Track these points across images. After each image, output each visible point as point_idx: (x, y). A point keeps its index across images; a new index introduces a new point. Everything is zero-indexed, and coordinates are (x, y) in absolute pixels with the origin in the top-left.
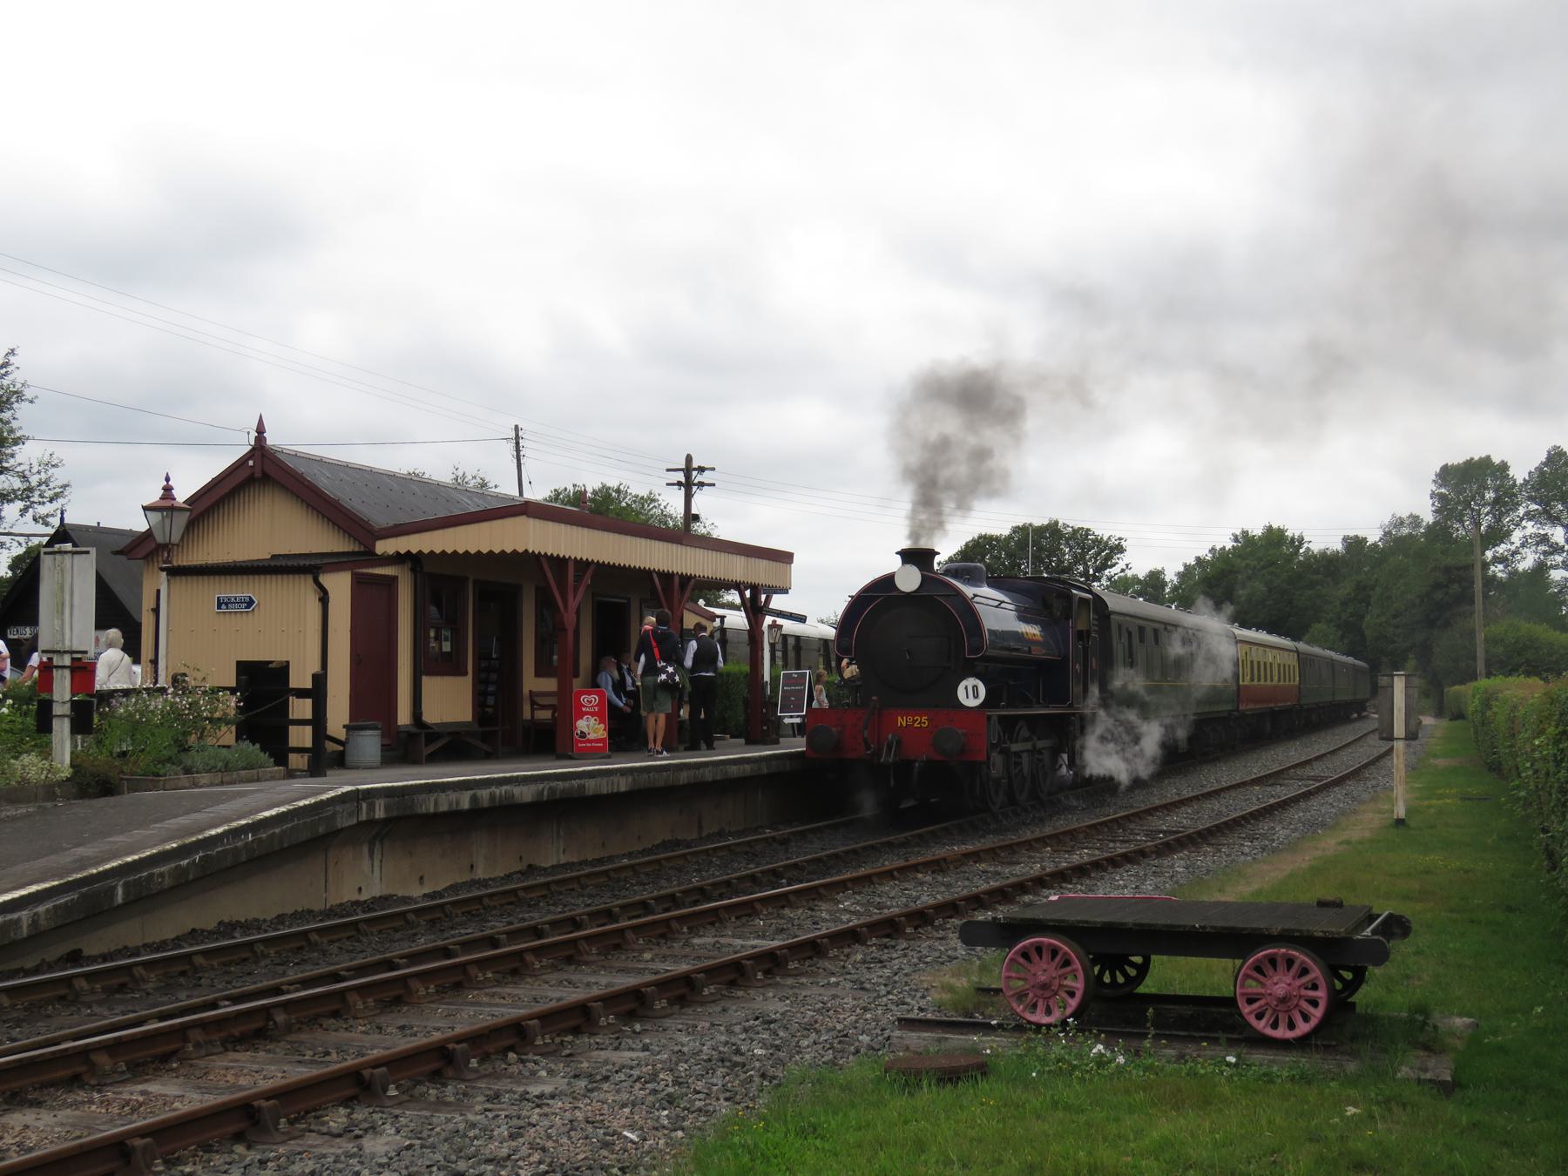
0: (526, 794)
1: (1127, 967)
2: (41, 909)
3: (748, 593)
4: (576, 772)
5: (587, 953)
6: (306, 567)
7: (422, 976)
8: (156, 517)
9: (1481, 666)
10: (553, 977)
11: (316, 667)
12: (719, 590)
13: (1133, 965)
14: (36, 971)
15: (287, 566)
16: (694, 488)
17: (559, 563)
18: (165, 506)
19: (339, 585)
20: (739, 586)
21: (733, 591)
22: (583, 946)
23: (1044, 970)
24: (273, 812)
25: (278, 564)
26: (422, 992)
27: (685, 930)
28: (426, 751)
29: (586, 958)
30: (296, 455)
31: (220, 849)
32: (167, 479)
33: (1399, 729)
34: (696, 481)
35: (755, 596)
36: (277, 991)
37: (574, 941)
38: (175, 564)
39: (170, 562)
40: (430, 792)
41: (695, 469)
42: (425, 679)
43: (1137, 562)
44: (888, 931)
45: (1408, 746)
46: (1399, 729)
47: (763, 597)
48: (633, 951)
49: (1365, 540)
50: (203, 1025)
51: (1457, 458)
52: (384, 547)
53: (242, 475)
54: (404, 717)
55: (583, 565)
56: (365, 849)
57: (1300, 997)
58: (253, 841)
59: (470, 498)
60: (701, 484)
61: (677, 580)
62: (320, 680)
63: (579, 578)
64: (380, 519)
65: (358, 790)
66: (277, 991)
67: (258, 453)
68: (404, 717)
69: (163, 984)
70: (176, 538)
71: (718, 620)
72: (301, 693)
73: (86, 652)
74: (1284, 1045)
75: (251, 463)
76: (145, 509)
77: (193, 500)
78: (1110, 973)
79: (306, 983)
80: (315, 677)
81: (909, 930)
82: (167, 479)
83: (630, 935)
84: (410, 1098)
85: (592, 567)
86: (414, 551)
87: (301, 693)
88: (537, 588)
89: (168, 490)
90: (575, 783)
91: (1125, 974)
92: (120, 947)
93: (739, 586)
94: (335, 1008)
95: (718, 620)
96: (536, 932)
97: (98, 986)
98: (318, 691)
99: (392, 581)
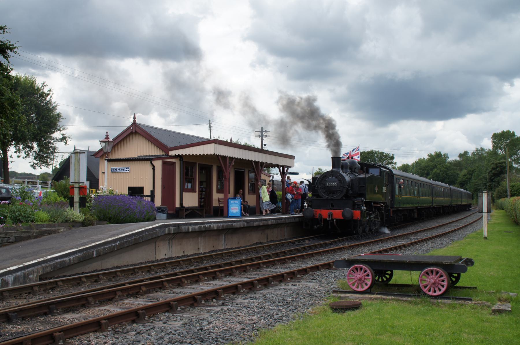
0: (215, 227)
1: (386, 275)
2: (72, 257)
3: (281, 168)
4: (230, 221)
5: (235, 273)
6: (149, 159)
7: (185, 278)
8: (104, 144)
9: (509, 193)
10: (225, 279)
11: (151, 189)
12: (269, 167)
13: (388, 274)
14: (70, 276)
15: (143, 159)
16: (264, 137)
17: (224, 158)
18: (106, 141)
19: (158, 164)
20: (278, 166)
21: (276, 168)
22: (234, 270)
23: (359, 275)
24: (140, 230)
25: (140, 158)
26: (186, 282)
27: (265, 266)
28: (185, 214)
29: (235, 274)
30: (145, 126)
31: (124, 241)
32: (107, 133)
33: (485, 209)
34: (264, 135)
35: (283, 169)
36: (142, 281)
37: (231, 269)
38: (109, 159)
39: (108, 158)
40: (187, 225)
41: (264, 131)
42: (184, 193)
43: (399, 161)
44: (328, 267)
45: (488, 215)
46: (485, 209)
47: (286, 169)
48: (249, 272)
49: (446, 156)
50: (121, 290)
51: (499, 131)
52: (172, 153)
53: (130, 131)
54: (177, 205)
55: (232, 159)
56: (167, 242)
57: (439, 283)
58: (134, 239)
59: (197, 139)
60: (266, 136)
61: (260, 163)
62: (153, 192)
63: (230, 163)
64: (171, 145)
65: (165, 224)
66: (142, 281)
67: (134, 125)
68: (177, 205)
69: (108, 280)
70: (109, 151)
71: (272, 177)
72: (147, 196)
73: (84, 183)
74: (436, 297)
75: (132, 128)
76: (100, 142)
77: (115, 139)
78: (381, 278)
79: (151, 279)
80: (151, 191)
81: (334, 267)
82: (107, 133)
83: (248, 268)
84: (183, 311)
85: (234, 159)
86: (180, 154)
87: (147, 196)
88: (217, 166)
89: (107, 136)
90: (230, 224)
91: (386, 277)
92: (95, 270)
93: (278, 166)
94: (160, 286)
95: (272, 177)
96: (219, 266)
97: (125, 294)
98: (152, 195)
99: (173, 164)
